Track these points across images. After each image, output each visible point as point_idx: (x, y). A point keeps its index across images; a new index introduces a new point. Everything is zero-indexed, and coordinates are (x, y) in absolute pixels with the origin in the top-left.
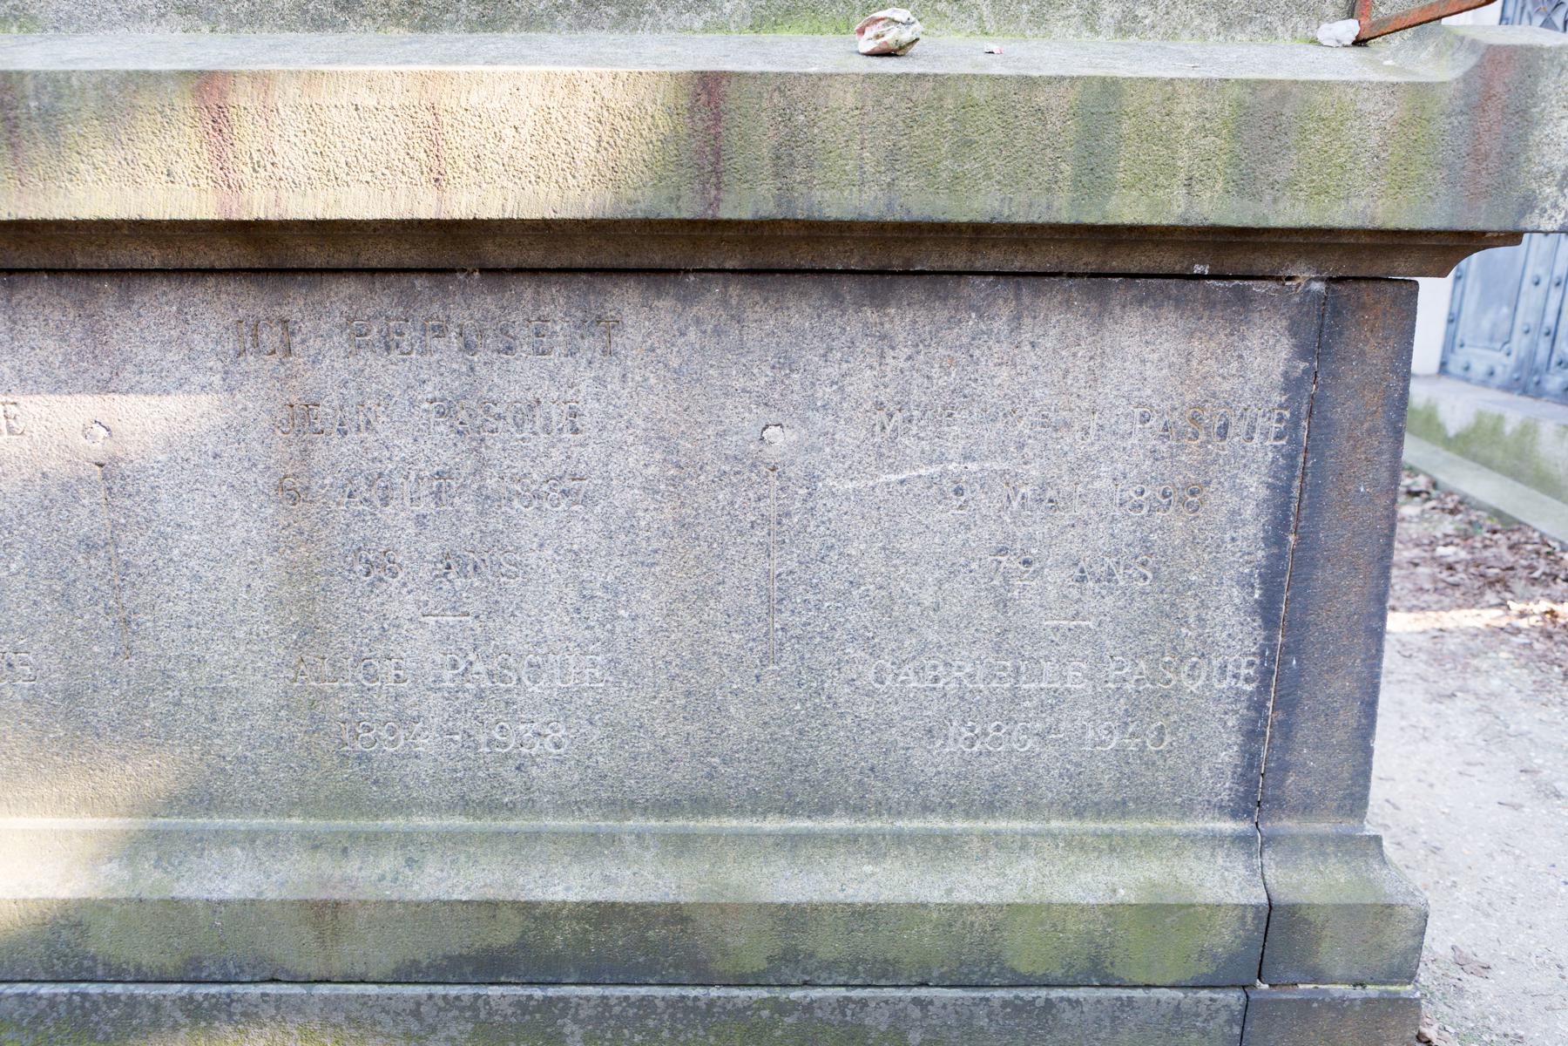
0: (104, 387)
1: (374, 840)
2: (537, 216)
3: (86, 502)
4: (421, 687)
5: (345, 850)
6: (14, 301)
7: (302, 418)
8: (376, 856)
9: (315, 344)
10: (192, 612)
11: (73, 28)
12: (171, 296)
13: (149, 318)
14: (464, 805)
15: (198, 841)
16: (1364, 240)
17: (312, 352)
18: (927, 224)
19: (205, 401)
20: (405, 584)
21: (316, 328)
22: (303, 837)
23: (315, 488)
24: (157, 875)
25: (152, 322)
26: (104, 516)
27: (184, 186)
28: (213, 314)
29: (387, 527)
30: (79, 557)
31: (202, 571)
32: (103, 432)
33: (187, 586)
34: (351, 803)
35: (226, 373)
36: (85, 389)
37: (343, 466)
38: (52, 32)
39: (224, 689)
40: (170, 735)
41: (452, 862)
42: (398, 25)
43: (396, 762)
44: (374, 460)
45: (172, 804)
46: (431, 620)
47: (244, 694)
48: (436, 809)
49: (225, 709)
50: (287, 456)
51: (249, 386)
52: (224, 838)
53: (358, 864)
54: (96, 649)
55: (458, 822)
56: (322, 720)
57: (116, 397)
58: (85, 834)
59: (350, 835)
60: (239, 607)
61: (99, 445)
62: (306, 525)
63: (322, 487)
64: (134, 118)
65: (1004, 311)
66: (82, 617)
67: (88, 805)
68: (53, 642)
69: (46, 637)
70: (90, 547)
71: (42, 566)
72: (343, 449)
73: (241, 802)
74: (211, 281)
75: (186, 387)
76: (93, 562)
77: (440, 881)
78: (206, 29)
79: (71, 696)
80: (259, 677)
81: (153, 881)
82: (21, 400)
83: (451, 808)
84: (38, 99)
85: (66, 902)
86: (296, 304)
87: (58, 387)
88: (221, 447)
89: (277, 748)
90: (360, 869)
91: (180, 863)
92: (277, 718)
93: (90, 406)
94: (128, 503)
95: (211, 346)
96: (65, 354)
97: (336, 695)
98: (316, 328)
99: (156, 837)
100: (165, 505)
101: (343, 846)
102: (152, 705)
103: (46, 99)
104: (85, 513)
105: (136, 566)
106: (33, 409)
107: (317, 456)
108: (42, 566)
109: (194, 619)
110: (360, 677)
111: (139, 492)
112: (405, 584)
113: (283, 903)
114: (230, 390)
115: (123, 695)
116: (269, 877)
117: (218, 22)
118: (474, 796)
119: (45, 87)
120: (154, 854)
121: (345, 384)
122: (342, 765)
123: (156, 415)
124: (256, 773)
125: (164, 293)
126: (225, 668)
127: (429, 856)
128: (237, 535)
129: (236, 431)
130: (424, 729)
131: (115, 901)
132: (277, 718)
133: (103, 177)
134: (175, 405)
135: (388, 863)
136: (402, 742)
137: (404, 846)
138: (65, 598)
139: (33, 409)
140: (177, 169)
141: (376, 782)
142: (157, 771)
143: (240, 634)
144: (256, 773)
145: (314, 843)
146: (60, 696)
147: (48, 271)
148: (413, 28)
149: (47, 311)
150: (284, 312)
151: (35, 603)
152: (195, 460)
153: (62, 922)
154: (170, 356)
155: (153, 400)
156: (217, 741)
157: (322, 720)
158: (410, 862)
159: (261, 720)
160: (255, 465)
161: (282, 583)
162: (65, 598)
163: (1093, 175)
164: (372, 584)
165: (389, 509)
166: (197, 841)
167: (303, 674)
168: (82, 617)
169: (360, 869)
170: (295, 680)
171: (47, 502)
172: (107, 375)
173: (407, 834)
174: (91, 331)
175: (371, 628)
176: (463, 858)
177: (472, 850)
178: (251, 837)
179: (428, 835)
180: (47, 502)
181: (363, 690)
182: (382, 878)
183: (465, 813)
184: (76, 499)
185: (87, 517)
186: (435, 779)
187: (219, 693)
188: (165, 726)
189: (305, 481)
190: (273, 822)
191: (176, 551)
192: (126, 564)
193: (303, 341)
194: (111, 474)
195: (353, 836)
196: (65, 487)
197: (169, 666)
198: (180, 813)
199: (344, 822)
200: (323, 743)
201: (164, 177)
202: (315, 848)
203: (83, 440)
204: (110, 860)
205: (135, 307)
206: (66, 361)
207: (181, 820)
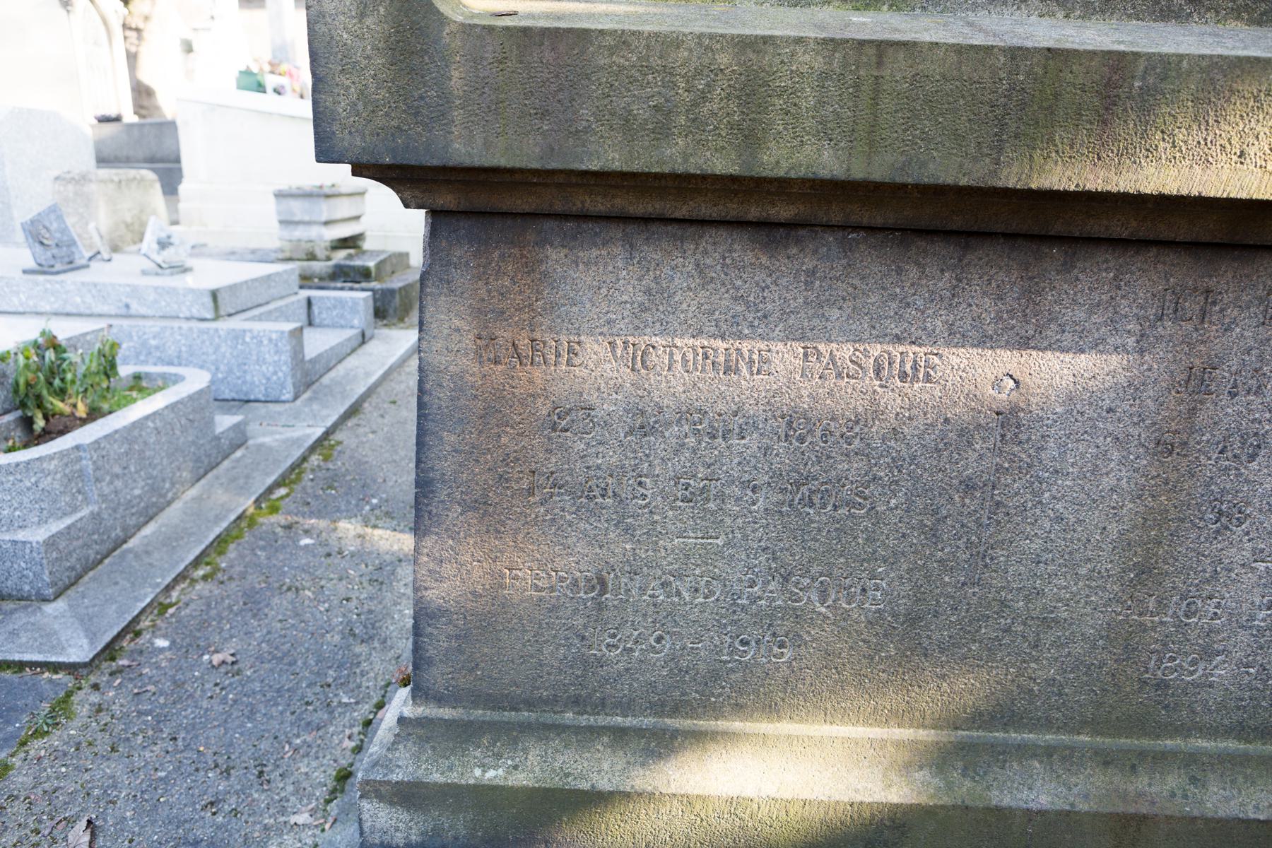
0: (1024, 344)
1: (1161, 760)
2: (1243, 195)
3: (977, 447)
4: (1234, 625)
5: (1133, 767)
6: (965, 261)
7: (1196, 382)
8: (1161, 773)
9: (1232, 312)
10: (1046, 550)
11: (939, 9)
12: (1111, 264)
13: (1085, 282)
14: (1240, 731)
15: (1001, 753)
16: (518, 177)
17: (1227, 320)
18: (803, 181)
19: (1115, 360)
20: (1248, 533)
21: (1237, 299)
22: (1096, 753)
23: (1192, 443)
24: (968, 783)
25: (1082, 289)
26: (992, 461)
27: (1252, 167)
28: (1144, 284)
29: (1247, 481)
30: (956, 497)
31: (1066, 512)
32: (1011, 383)
33: (1047, 525)
34: (1140, 724)
35: (1142, 336)
36: (1008, 345)
37: (1224, 426)
38: (918, 11)
39: (1053, 620)
40: (991, 658)
41: (1232, 781)
42: (1237, 19)
43: (1190, 689)
44: (1253, 421)
45: (978, 719)
46: (1261, 566)
47: (1071, 624)
48: (1213, 732)
49: (1049, 638)
50: (1175, 414)
51: (1160, 350)
52: (1024, 752)
53: (1146, 780)
54: (947, 579)
55: (1232, 745)
56: (1135, 649)
57: (1034, 353)
58: (898, 744)
59: (1140, 754)
60: (1090, 547)
61: (1004, 396)
62: (1173, 476)
63: (1198, 443)
64: (1228, 101)
65: (531, 236)
66: (942, 550)
67: (899, 717)
68: (909, 571)
69: (905, 566)
70: (968, 486)
71: (920, 503)
72: (1230, 411)
73: (1038, 720)
74: (1153, 251)
75: (1101, 347)
76: (967, 501)
77: (1227, 800)
78: (1060, 15)
79: (913, 619)
80: (1089, 609)
81: (965, 789)
82: (945, 352)
83: (1228, 732)
84: (1143, 78)
85: (897, 806)
86: (1226, 280)
87: (985, 341)
88: (1117, 402)
89: (1086, 673)
90: (1150, 785)
91: (985, 773)
92: (1094, 647)
93: (1009, 360)
94: (1016, 449)
95: (1135, 311)
96: (997, 313)
97: (1154, 629)
98: (1237, 299)
99: (962, 749)
100: (1052, 449)
101: (1132, 763)
102: (983, 631)
103: (1151, 80)
104: (973, 456)
105: (1006, 506)
106: (955, 360)
107: (1202, 416)
108: (920, 503)
109: (1045, 556)
110: (1181, 613)
111: (1029, 439)
112: (1248, 533)
113: (1096, 815)
114: (1141, 352)
115: (960, 621)
116: (1070, 789)
117: (1073, 9)
118: (1251, 722)
119: (1154, 69)
120: (960, 764)
121: (1249, 351)
122: (1140, 690)
123: (1065, 371)
124: (1060, 694)
125: (1106, 261)
126: (1060, 600)
127: (1211, 776)
128: (1107, 482)
129: (1134, 389)
130: (1224, 662)
131: (942, 807)
132: (1094, 647)
133: (1178, 155)
134: (1085, 362)
135: (1174, 781)
136: (1200, 672)
137: (1187, 766)
138: (933, 535)
139: (955, 360)
140: (1251, 151)
141: (1166, 707)
142: (969, 687)
143: (1083, 571)
144: (1060, 694)
145: (1106, 760)
146: (902, 619)
147: (1005, 235)
148: (1251, 22)
149: (992, 272)
150: (1212, 283)
151: (904, 535)
152: (1090, 413)
153: (888, 824)
154: (1095, 318)
155: (1068, 358)
156: (1033, 665)
157: (1135, 649)
158: (1193, 780)
159: (1077, 649)
160: (1143, 420)
161: (1135, 527)
162: (933, 535)
163: (750, 138)
164: (1218, 532)
165: (1254, 465)
166: (1000, 754)
167: (1129, 608)
168: (942, 550)
169: (1150, 785)
170: (1120, 614)
171: (941, 446)
172: (1031, 332)
173: (1191, 755)
174: (1027, 293)
175: (1204, 571)
176: (1241, 780)
177: (1249, 771)
178: (1049, 752)
179: (1211, 756)
180: (941, 446)
181: (1180, 625)
182: (1173, 795)
183: (1239, 738)
184: (970, 444)
185: (972, 463)
186: (1222, 706)
187: (1047, 623)
188: (990, 649)
189: (1185, 436)
190: (1064, 738)
191: (1047, 495)
192: (998, 504)
193: (1222, 310)
194: (1009, 420)
195: (1142, 754)
196: (962, 433)
197: (1009, 597)
198: (980, 727)
199: (1129, 741)
200: (1129, 671)
201: (1235, 158)
202: (1106, 764)
203: (991, 392)
204: (921, 768)
205: (1076, 271)
206: (999, 318)
207: (980, 733)
